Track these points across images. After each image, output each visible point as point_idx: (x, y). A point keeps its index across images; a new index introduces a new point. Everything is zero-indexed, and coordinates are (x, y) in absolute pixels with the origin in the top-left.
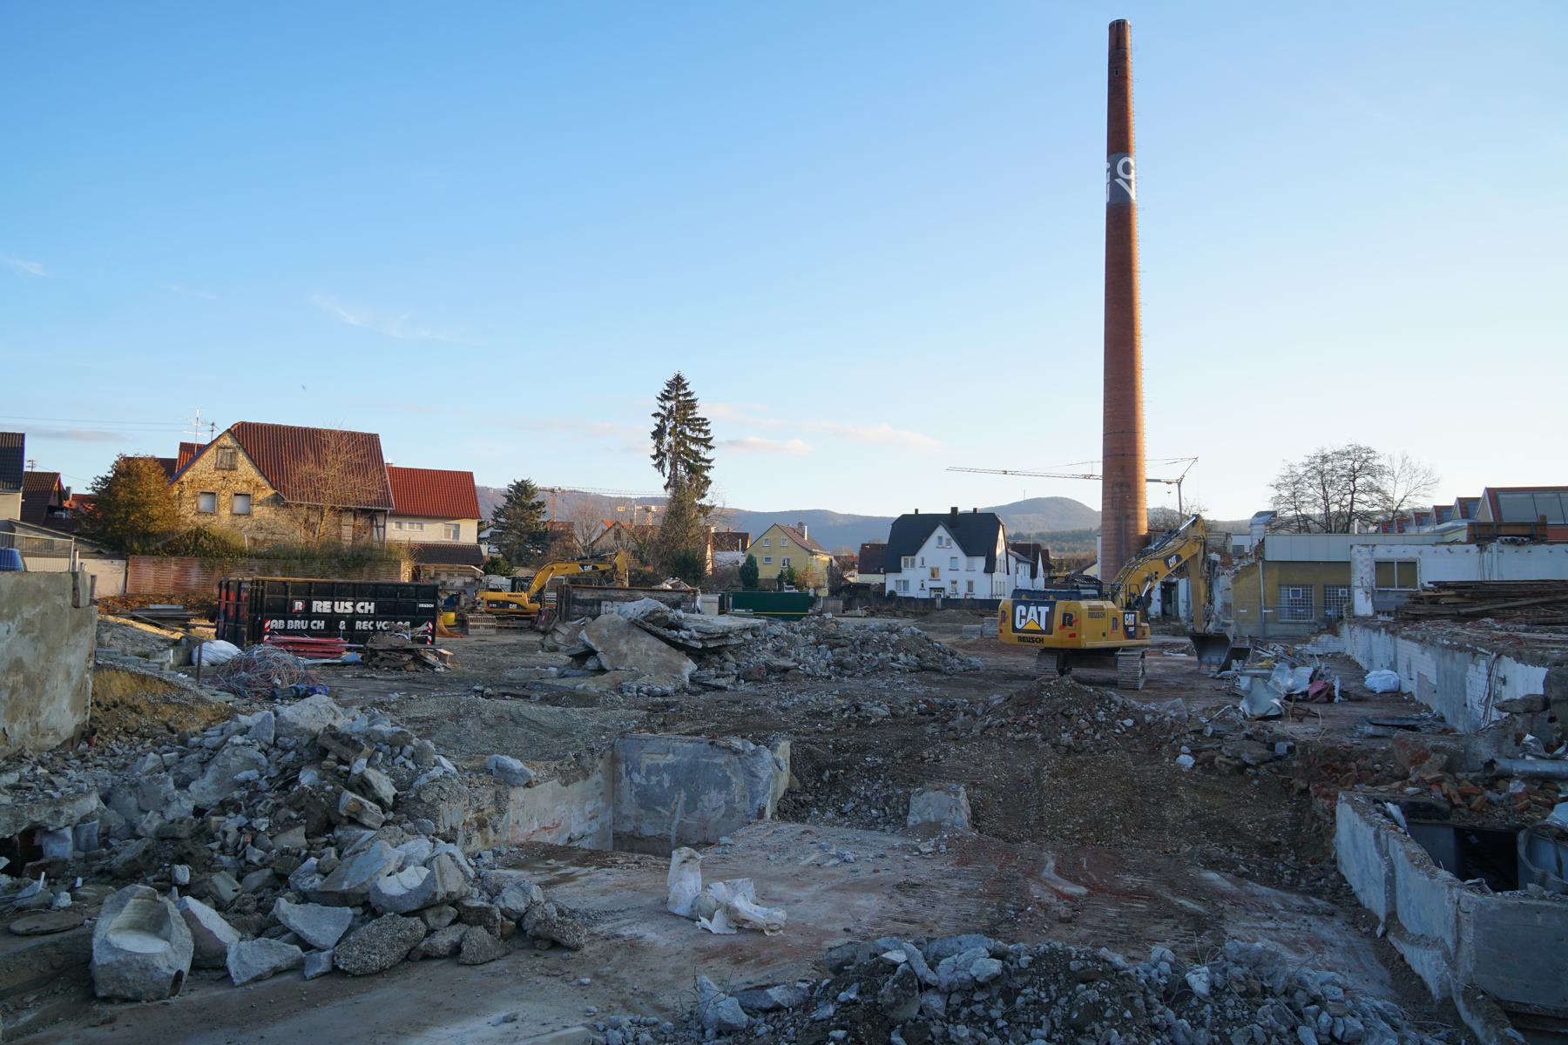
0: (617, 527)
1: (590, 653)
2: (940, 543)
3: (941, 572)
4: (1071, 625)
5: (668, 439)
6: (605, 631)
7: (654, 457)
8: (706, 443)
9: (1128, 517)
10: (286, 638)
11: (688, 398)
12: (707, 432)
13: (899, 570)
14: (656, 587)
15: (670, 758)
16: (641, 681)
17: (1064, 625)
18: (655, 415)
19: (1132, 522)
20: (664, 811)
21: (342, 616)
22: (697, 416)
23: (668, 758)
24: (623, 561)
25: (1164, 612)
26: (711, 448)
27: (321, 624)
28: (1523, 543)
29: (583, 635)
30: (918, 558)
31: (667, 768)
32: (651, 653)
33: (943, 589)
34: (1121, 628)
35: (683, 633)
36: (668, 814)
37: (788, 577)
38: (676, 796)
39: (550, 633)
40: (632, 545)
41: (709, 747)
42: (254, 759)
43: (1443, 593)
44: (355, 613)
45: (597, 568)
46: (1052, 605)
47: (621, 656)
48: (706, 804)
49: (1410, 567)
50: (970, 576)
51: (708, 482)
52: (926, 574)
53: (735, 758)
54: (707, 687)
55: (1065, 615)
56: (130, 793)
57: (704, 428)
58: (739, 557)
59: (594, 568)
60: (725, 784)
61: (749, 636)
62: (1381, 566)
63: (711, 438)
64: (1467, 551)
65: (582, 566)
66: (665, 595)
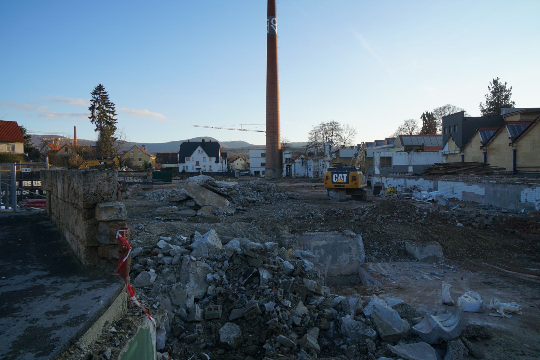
0: (66, 146)
2: (199, 152)
3: (200, 163)
4: (355, 180)
6: (193, 190)
7: (90, 118)
8: (112, 112)
10: (38, 200)
11: (105, 94)
12: (113, 108)
13: (184, 162)
15: (324, 242)
17: (353, 180)
18: (91, 100)
19: (276, 145)
20: (322, 264)
21: (37, 188)
22: (109, 102)
23: (323, 242)
25: (287, 175)
26: (115, 115)
28: (420, 151)
30: (191, 158)
31: (323, 246)
32: (213, 198)
33: (201, 169)
36: (324, 265)
38: (327, 258)
39: (125, 191)
41: (342, 236)
42: (206, 267)
43: (440, 167)
45: (106, 163)
46: (348, 173)
47: (203, 200)
48: (341, 259)
49: (389, 159)
50: (210, 164)
51: (115, 129)
52: (194, 164)
53: (352, 240)
55: (353, 177)
56: (165, 297)
57: (112, 106)
59: (105, 163)
60: (349, 250)
62: (382, 159)
63: (115, 111)
64: (405, 154)
65: (100, 162)
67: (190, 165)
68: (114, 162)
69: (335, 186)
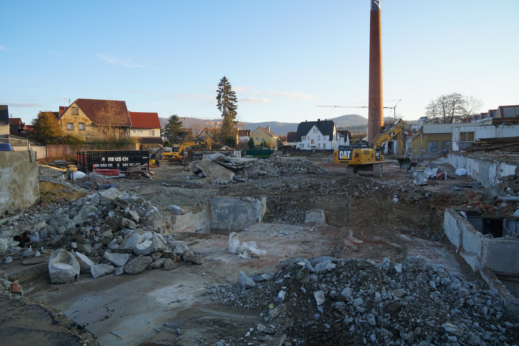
0: (207, 129)
1: (200, 171)
2: (314, 131)
5: (222, 99)
6: (204, 164)
7: (218, 106)
8: (235, 100)
9: (377, 120)
12: (235, 96)
13: (301, 141)
14: (220, 149)
15: (228, 204)
16: (217, 180)
17: (356, 157)
18: (217, 91)
19: (378, 122)
21: (118, 162)
22: (231, 91)
24: (209, 141)
26: (236, 102)
27: (111, 165)
28: (511, 124)
29: (197, 165)
30: (307, 136)
31: (227, 207)
34: (374, 157)
35: (230, 164)
37: (264, 144)
40: (212, 135)
44: (122, 161)
46: (352, 150)
47: (210, 172)
49: (472, 134)
50: (324, 142)
51: (236, 113)
52: (310, 142)
53: (248, 204)
54: (239, 181)
55: (356, 154)
57: (234, 95)
58: (247, 138)
59: (200, 143)
60: (246, 212)
61: (252, 164)
62: (462, 134)
64: (492, 128)
65: (196, 143)
66: (224, 152)
67: (305, 144)
68: (206, 143)
69: (341, 162)
